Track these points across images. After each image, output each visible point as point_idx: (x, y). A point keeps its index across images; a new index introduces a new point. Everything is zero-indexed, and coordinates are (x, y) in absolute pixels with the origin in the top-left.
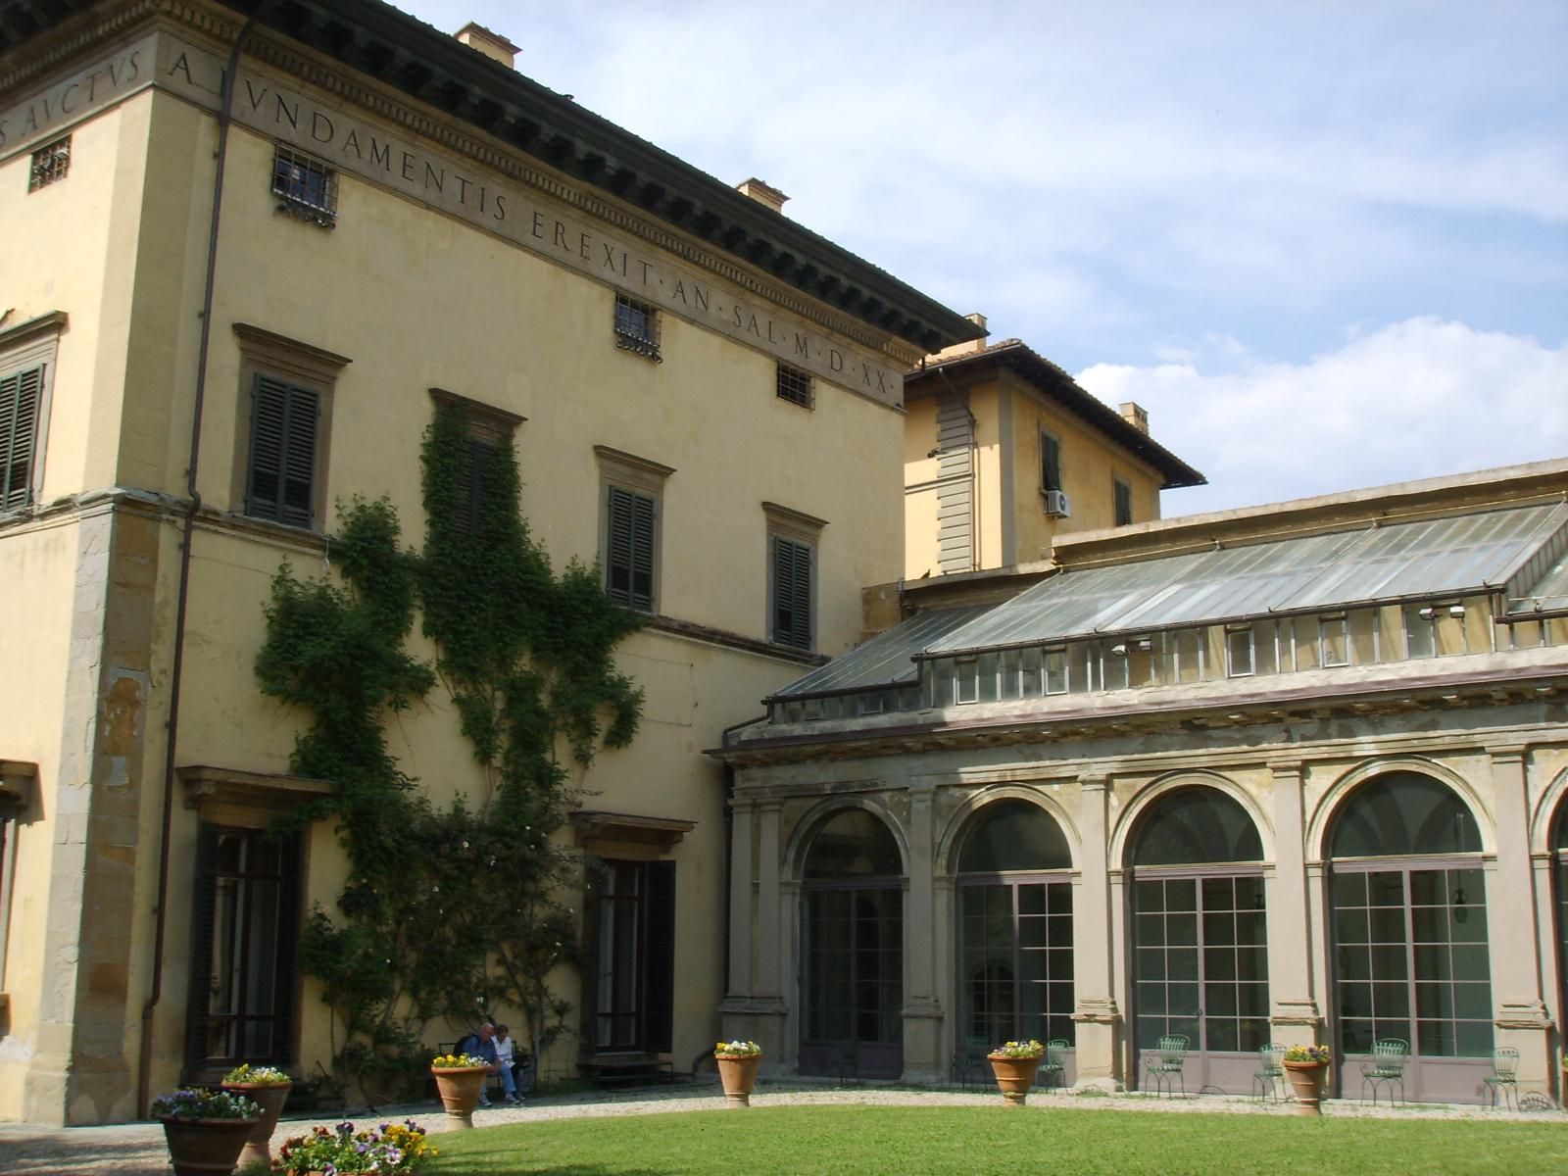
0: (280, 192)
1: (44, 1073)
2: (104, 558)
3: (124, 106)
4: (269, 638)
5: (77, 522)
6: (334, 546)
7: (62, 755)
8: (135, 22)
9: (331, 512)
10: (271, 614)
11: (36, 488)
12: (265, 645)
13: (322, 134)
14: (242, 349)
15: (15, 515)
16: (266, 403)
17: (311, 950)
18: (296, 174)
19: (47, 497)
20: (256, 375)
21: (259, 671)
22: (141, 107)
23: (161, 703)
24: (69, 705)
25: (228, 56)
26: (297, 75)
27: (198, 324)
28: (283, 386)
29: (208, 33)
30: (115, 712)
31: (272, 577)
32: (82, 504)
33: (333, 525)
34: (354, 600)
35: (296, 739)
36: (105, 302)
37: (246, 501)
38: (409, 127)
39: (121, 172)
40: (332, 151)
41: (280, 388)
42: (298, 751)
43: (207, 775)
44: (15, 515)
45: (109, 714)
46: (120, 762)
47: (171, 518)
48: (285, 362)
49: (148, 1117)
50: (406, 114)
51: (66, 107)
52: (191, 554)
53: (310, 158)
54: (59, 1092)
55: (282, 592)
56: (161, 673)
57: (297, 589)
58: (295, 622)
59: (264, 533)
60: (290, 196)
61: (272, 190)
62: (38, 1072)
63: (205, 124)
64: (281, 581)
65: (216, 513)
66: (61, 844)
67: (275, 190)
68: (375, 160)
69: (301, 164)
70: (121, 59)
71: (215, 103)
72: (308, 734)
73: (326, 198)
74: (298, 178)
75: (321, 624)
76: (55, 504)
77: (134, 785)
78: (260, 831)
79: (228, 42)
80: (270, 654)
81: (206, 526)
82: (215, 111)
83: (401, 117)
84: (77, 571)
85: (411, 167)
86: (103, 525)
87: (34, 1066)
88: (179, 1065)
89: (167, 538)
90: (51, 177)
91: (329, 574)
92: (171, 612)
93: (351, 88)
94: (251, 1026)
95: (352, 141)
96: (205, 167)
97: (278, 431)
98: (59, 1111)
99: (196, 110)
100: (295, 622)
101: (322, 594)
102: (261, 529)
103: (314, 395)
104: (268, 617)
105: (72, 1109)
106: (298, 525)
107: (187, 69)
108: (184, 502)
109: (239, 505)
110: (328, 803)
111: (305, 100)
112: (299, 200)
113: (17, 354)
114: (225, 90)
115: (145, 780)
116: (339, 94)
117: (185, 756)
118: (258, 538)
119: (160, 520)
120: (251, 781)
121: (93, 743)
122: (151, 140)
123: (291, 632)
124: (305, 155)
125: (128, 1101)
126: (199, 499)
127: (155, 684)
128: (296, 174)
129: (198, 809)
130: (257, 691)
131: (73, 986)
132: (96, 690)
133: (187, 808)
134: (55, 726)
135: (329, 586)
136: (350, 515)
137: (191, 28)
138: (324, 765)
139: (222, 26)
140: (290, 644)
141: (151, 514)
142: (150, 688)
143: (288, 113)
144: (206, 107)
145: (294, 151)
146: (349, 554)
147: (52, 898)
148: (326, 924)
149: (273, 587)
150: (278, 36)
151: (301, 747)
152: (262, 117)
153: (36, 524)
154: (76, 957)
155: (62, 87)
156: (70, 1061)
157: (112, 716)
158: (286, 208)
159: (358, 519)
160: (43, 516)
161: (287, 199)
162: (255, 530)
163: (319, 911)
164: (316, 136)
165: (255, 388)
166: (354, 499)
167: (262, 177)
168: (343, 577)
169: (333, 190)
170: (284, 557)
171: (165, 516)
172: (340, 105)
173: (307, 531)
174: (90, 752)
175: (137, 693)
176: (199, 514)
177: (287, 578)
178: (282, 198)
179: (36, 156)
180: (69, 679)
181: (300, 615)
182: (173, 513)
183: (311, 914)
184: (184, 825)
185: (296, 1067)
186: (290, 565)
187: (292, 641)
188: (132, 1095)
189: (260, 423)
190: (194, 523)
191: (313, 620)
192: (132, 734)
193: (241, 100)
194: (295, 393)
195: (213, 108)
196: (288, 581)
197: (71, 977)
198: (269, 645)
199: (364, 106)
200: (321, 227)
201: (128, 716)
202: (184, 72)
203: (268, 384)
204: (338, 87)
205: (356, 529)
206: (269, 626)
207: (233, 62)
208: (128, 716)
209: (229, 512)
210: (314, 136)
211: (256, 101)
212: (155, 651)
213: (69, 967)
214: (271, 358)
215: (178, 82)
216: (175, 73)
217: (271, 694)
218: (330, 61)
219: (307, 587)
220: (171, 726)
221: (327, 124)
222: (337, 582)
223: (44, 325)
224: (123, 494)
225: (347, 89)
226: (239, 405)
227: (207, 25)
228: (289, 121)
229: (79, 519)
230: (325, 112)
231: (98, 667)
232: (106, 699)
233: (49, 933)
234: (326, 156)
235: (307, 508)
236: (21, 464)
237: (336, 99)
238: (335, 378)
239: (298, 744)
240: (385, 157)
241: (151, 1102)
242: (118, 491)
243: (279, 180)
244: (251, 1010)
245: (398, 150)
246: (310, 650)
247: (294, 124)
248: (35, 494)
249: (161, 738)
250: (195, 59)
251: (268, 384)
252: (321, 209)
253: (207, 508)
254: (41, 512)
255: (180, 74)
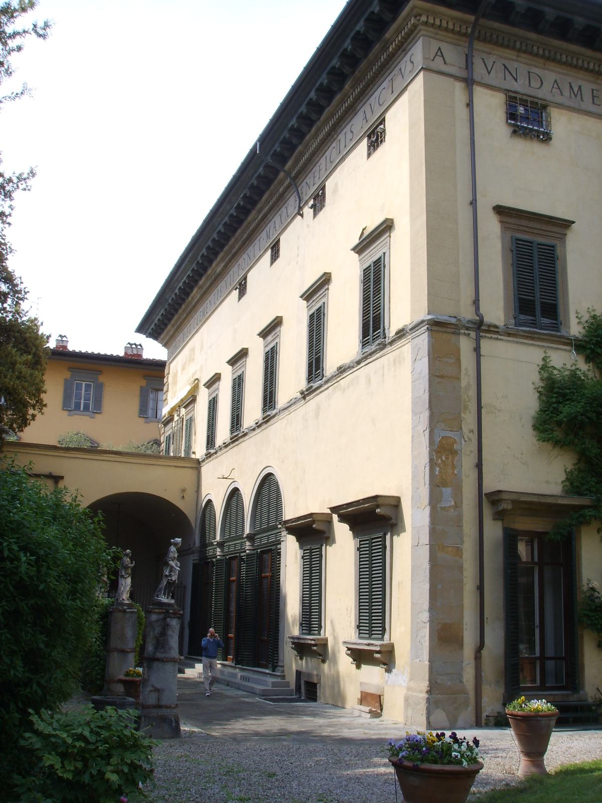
0: (513, 122)
1: (414, 694)
2: (426, 360)
3: (409, 88)
4: (540, 406)
5: (410, 342)
6: (578, 343)
7: (412, 489)
8: (408, 35)
9: (573, 321)
10: (540, 389)
11: (386, 328)
12: (538, 410)
13: (535, 83)
14: (501, 222)
15: (376, 346)
16: (520, 254)
17: (586, 612)
18: (521, 110)
19: (391, 332)
20: (512, 237)
21: (535, 427)
22: (418, 85)
23: (471, 452)
24: (414, 458)
25: (467, 44)
26: (513, 48)
27: (470, 209)
28: (531, 243)
29: (453, 31)
30: (442, 459)
31: (538, 365)
32: (411, 330)
33: (575, 329)
34: (596, 377)
35: (566, 471)
36: (411, 205)
37: (515, 318)
38: (592, 71)
39: (412, 126)
40: (544, 93)
41: (529, 244)
42: (567, 479)
43: (505, 496)
44: (376, 346)
45: (437, 460)
46: (447, 491)
47: (466, 332)
48: (530, 228)
49: (483, 724)
50: (589, 63)
51: (381, 104)
52: (482, 353)
53: (529, 99)
54: (423, 707)
55: (546, 375)
56: (469, 432)
57: (555, 372)
58: (556, 393)
59: (530, 337)
60: (519, 124)
61: (507, 121)
62: (410, 693)
63: (459, 87)
64: (544, 368)
65: (496, 327)
66: (415, 546)
67: (509, 121)
68: (573, 96)
69: (524, 103)
70: (405, 64)
71: (464, 74)
72: (573, 467)
73: (544, 123)
74: (523, 112)
75: (573, 393)
76: (397, 333)
77: (458, 506)
78: (546, 533)
79: (465, 35)
80: (541, 414)
81: (490, 335)
82: (463, 79)
83: (586, 65)
84: (412, 373)
85: (598, 97)
86: (423, 340)
87: (409, 689)
88: (502, 690)
89: (465, 344)
90: (378, 146)
91: (576, 361)
92: (473, 392)
93: (550, 52)
94: (550, 664)
95: (556, 86)
96: (462, 113)
97: (531, 271)
98: (424, 719)
99: (452, 80)
100: (556, 393)
101: (573, 374)
102: (526, 334)
103: (553, 247)
104: (539, 392)
105: (432, 718)
106: (554, 331)
107: (442, 56)
108: (473, 321)
109: (512, 321)
110: (589, 512)
111: (520, 66)
112: (526, 125)
113: (370, 252)
114: (469, 64)
115: (465, 502)
116: (542, 57)
117: (490, 485)
118: (525, 341)
119: (459, 334)
120: (535, 499)
121: (428, 480)
122: (425, 101)
123: (554, 400)
124: (525, 98)
125: (468, 713)
126: (483, 318)
127: (466, 439)
128: (521, 110)
129: (502, 520)
130: (534, 440)
131: (427, 638)
132: (428, 445)
133: (494, 519)
134: (407, 471)
135: (577, 369)
136: (587, 322)
137: (441, 30)
138: (585, 487)
139: (460, 26)
140: (553, 408)
141: (453, 330)
142: (463, 442)
143: (511, 74)
144: (458, 77)
145: (518, 96)
146: (588, 346)
147: (412, 581)
148: (596, 594)
149: (540, 372)
150: (496, 25)
151: (569, 476)
152: (495, 78)
153: (388, 349)
154: (428, 619)
155: (377, 94)
156: (428, 687)
157: (440, 461)
158: (517, 132)
159: (592, 324)
160: (391, 343)
161: (518, 126)
162: (523, 336)
163: (590, 586)
164: (531, 86)
165: (512, 245)
166: (588, 311)
167: (499, 114)
168: (586, 363)
169: (548, 117)
170: (545, 352)
171: (462, 331)
172: (545, 64)
173: (559, 334)
174: (427, 486)
175: (455, 446)
176: (483, 328)
177: (548, 366)
178: (514, 125)
179: (369, 137)
180: (412, 441)
181: (559, 388)
182: (467, 329)
183: (585, 588)
184: (494, 531)
185: (581, 692)
186: (549, 357)
187: (555, 405)
188: (471, 709)
189: (519, 274)
190: (481, 334)
191: (568, 391)
192: (453, 473)
193: (479, 70)
194: (539, 246)
195: (461, 76)
196: (548, 367)
197: (426, 632)
198: (541, 410)
199: (560, 62)
200: (542, 141)
201: (450, 460)
202: (441, 58)
203: (520, 242)
204: (541, 52)
205: (591, 330)
206: (539, 397)
207: (471, 47)
208: (450, 460)
209: (505, 326)
210: (530, 86)
211: (489, 70)
212: (464, 418)
213: (425, 625)
214: (521, 226)
215: (438, 64)
216: (435, 59)
217: (544, 441)
218: (533, 36)
219: (562, 370)
220: (479, 466)
221: (539, 79)
222: (583, 366)
223: (380, 229)
224: (433, 318)
225: (547, 52)
226: (504, 257)
227: (451, 26)
228: (513, 79)
229: (410, 339)
230: (534, 70)
231: (428, 431)
232: (435, 450)
233: (412, 603)
234: (540, 96)
235: (556, 319)
236: (377, 315)
237: (541, 60)
238: (565, 235)
239: (567, 475)
240: (579, 93)
241: (484, 715)
242: (430, 317)
243: (512, 115)
244: (550, 652)
245: (587, 87)
246: (567, 410)
247: (516, 80)
248: (386, 331)
249: (474, 475)
250: (448, 50)
251: (520, 242)
252: (541, 129)
253: (489, 323)
254: (389, 341)
255: (439, 60)
